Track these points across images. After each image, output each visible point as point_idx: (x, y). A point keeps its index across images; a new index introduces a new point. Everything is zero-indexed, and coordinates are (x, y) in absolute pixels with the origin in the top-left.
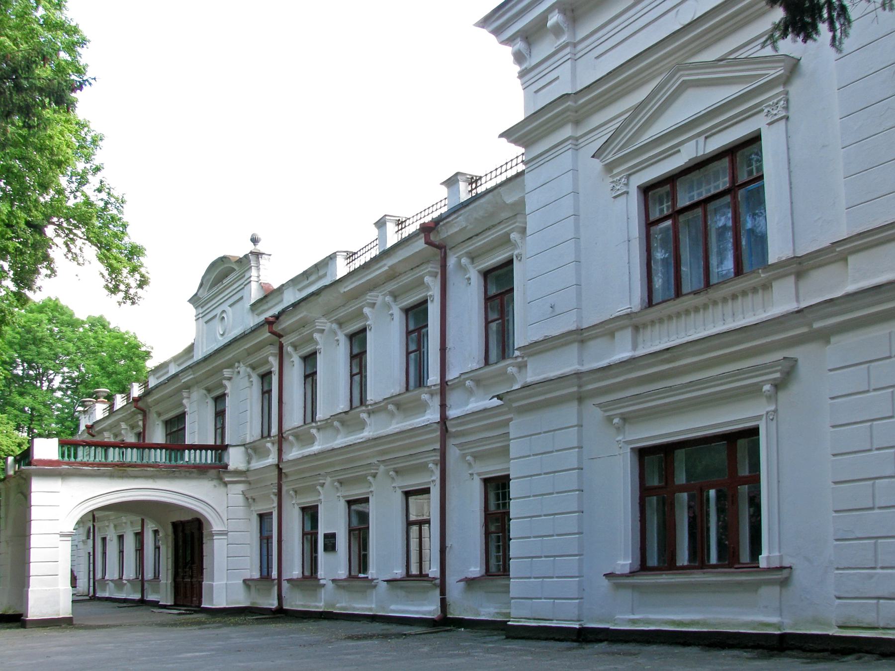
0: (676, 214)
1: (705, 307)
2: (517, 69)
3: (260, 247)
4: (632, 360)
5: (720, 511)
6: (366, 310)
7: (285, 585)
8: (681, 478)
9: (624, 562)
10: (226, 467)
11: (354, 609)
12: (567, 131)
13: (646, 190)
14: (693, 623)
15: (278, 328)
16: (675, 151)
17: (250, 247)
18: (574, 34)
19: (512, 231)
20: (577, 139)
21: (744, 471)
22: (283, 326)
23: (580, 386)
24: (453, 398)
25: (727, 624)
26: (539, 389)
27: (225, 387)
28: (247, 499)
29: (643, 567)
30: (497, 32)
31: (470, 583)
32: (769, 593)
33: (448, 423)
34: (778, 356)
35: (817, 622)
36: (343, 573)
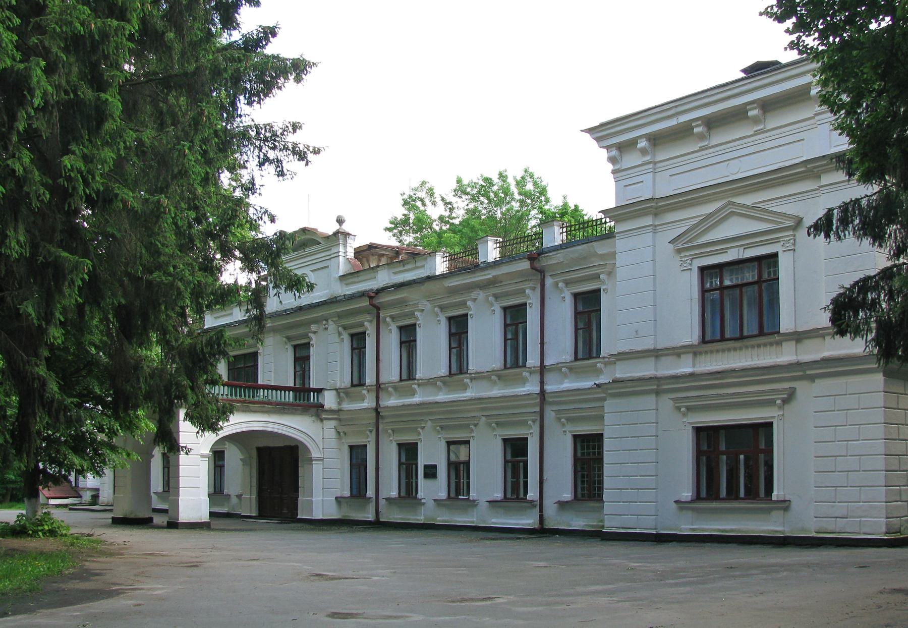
0: (722, 288)
1: (741, 349)
2: (610, 167)
3: (346, 227)
4: (692, 375)
5: (747, 466)
6: (469, 303)
7: (382, 502)
8: (723, 447)
9: (687, 494)
10: (322, 406)
11: (456, 522)
12: (648, 221)
13: (703, 270)
14: (732, 531)
15: (377, 301)
16: (724, 251)
17: (335, 227)
18: (654, 156)
19: (602, 273)
20: (656, 226)
21: (762, 446)
22: (381, 300)
23: (658, 386)
24: (548, 377)
25: (753, 531)
26: (629, 384)
27: (311, 339)
28: (339, 433)
29: (698, 498)
30: (598, 140)
31: (562, 505)
32: (776, 515)
33: (546, 396)
34: (786, 385)
35: (803, 530)
36: (443, 495)
